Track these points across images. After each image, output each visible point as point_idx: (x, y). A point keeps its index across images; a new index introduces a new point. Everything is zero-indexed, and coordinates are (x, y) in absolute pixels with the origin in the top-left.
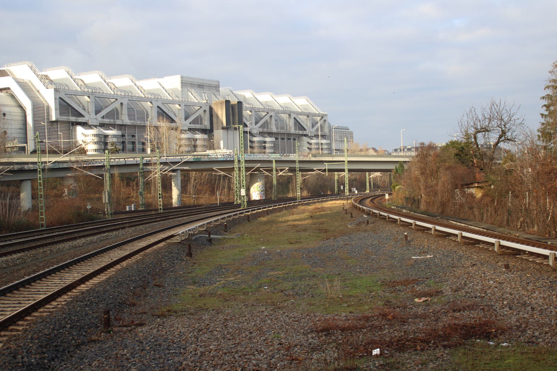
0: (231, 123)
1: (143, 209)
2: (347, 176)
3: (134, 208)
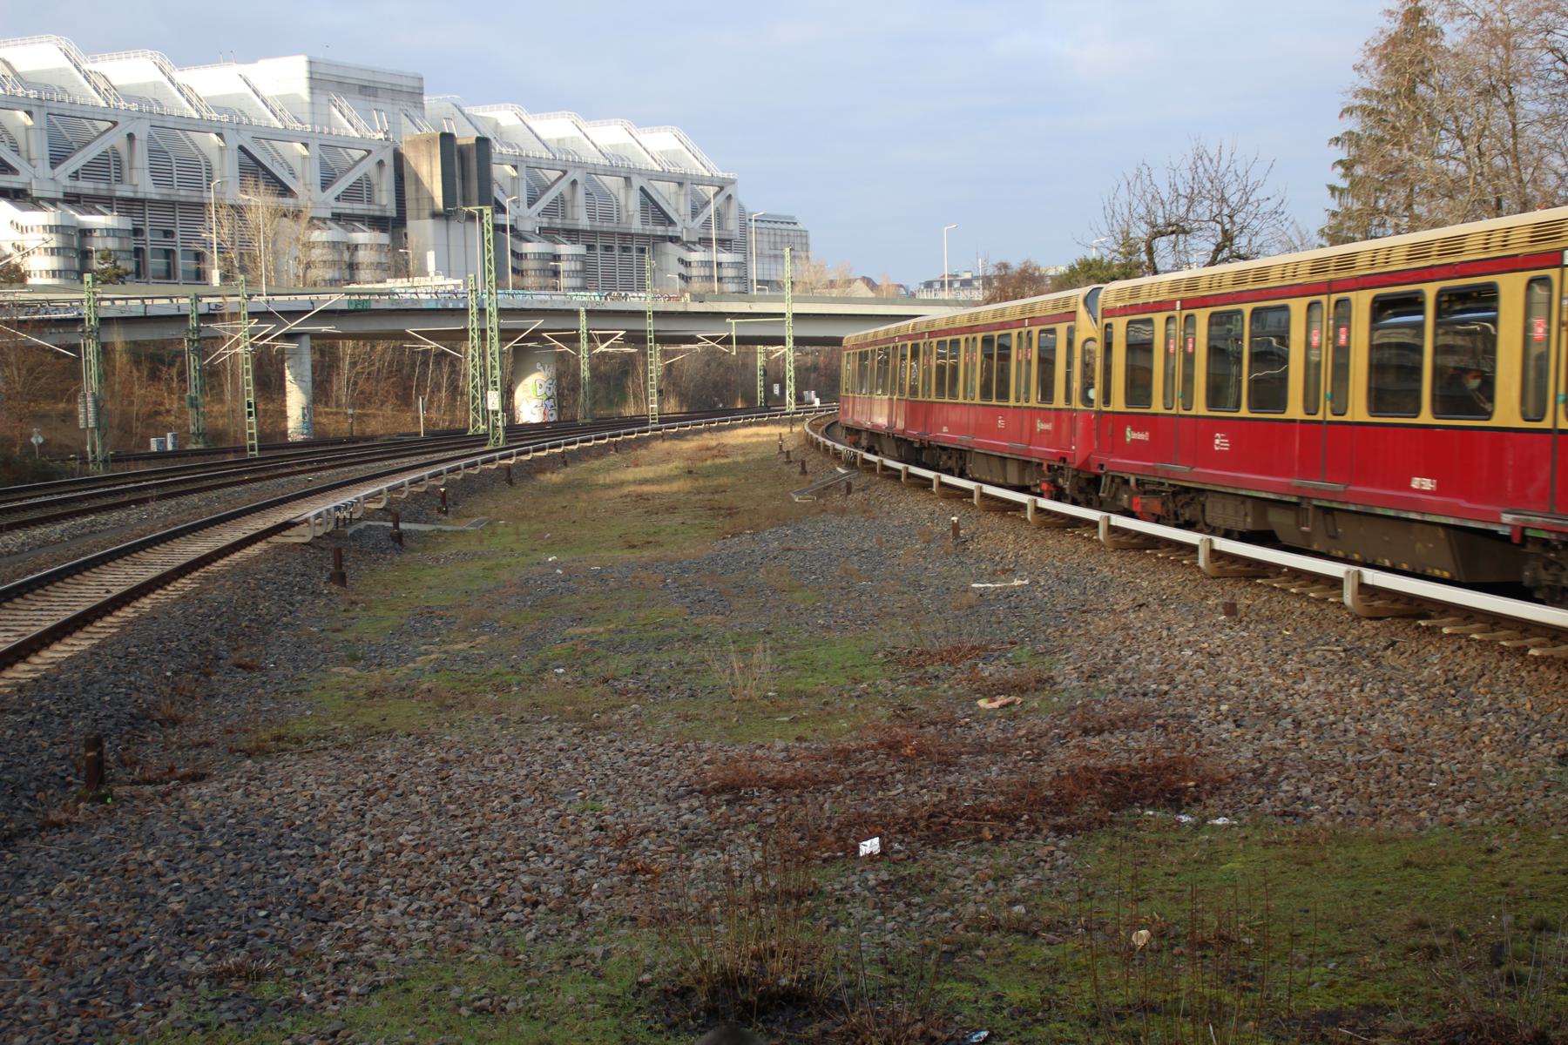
0: (459, 201)
1: (200, 446)
2: (790, 358)
3: (174, 445)
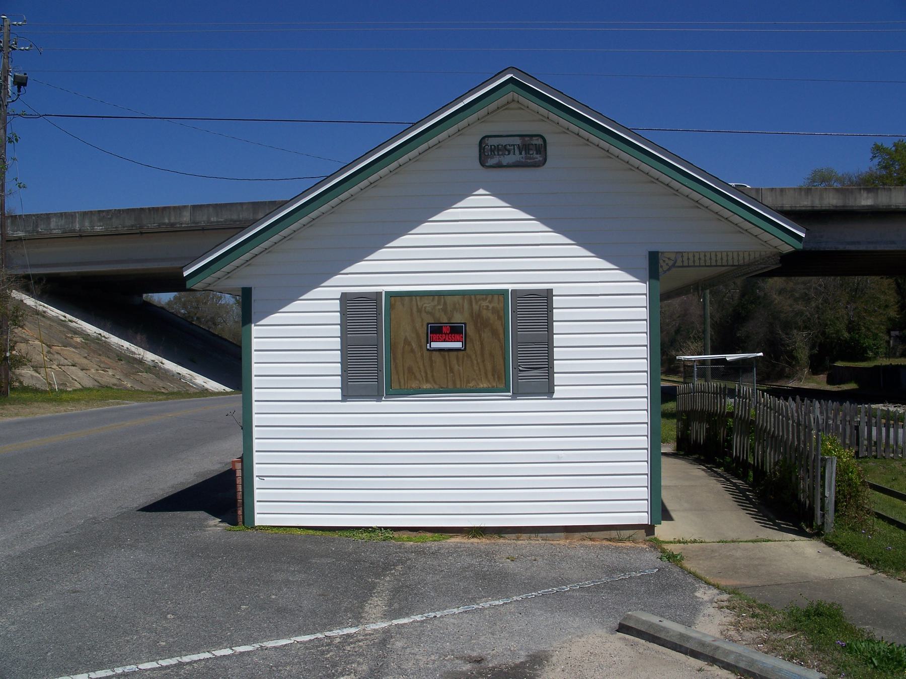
3: (519, 334)
